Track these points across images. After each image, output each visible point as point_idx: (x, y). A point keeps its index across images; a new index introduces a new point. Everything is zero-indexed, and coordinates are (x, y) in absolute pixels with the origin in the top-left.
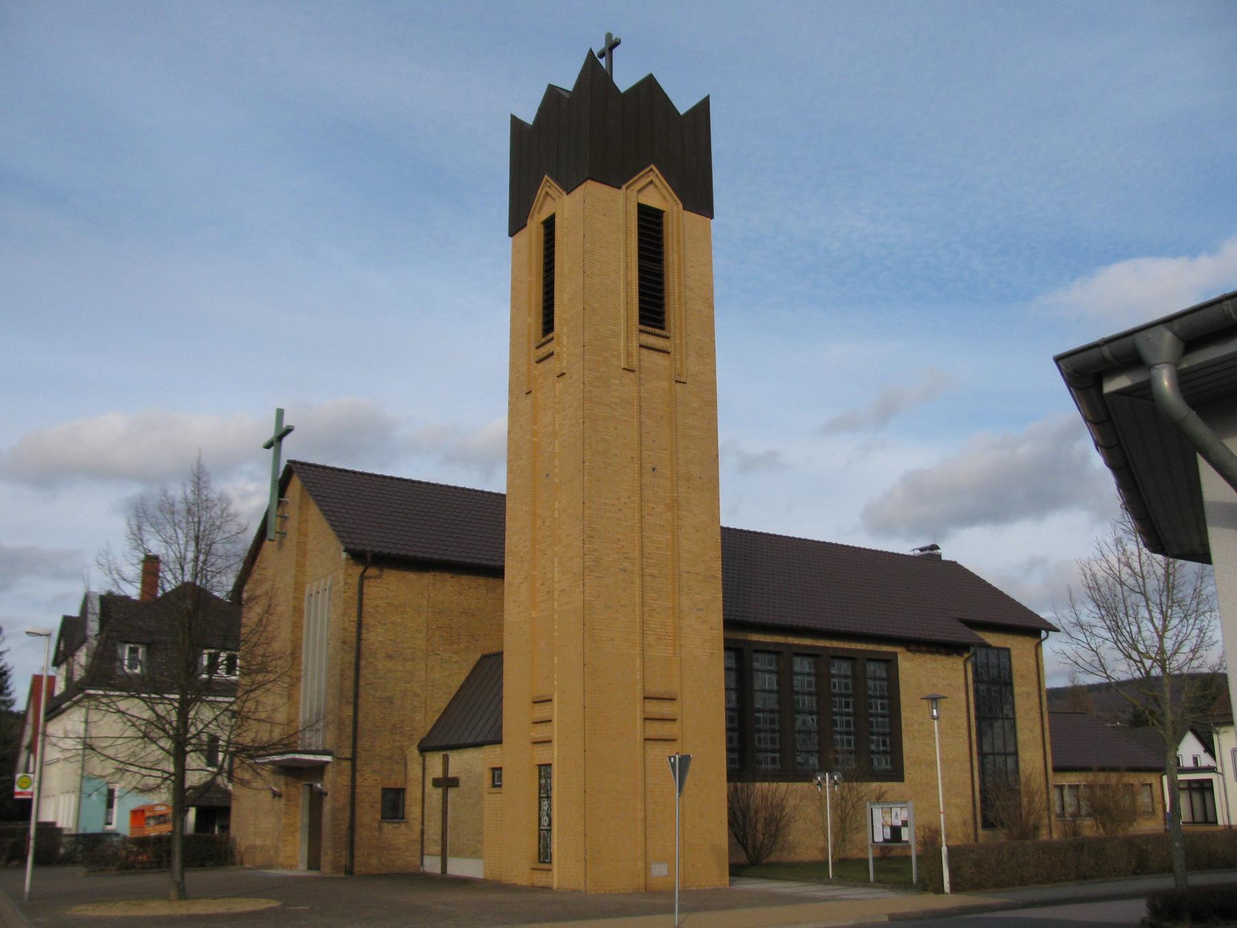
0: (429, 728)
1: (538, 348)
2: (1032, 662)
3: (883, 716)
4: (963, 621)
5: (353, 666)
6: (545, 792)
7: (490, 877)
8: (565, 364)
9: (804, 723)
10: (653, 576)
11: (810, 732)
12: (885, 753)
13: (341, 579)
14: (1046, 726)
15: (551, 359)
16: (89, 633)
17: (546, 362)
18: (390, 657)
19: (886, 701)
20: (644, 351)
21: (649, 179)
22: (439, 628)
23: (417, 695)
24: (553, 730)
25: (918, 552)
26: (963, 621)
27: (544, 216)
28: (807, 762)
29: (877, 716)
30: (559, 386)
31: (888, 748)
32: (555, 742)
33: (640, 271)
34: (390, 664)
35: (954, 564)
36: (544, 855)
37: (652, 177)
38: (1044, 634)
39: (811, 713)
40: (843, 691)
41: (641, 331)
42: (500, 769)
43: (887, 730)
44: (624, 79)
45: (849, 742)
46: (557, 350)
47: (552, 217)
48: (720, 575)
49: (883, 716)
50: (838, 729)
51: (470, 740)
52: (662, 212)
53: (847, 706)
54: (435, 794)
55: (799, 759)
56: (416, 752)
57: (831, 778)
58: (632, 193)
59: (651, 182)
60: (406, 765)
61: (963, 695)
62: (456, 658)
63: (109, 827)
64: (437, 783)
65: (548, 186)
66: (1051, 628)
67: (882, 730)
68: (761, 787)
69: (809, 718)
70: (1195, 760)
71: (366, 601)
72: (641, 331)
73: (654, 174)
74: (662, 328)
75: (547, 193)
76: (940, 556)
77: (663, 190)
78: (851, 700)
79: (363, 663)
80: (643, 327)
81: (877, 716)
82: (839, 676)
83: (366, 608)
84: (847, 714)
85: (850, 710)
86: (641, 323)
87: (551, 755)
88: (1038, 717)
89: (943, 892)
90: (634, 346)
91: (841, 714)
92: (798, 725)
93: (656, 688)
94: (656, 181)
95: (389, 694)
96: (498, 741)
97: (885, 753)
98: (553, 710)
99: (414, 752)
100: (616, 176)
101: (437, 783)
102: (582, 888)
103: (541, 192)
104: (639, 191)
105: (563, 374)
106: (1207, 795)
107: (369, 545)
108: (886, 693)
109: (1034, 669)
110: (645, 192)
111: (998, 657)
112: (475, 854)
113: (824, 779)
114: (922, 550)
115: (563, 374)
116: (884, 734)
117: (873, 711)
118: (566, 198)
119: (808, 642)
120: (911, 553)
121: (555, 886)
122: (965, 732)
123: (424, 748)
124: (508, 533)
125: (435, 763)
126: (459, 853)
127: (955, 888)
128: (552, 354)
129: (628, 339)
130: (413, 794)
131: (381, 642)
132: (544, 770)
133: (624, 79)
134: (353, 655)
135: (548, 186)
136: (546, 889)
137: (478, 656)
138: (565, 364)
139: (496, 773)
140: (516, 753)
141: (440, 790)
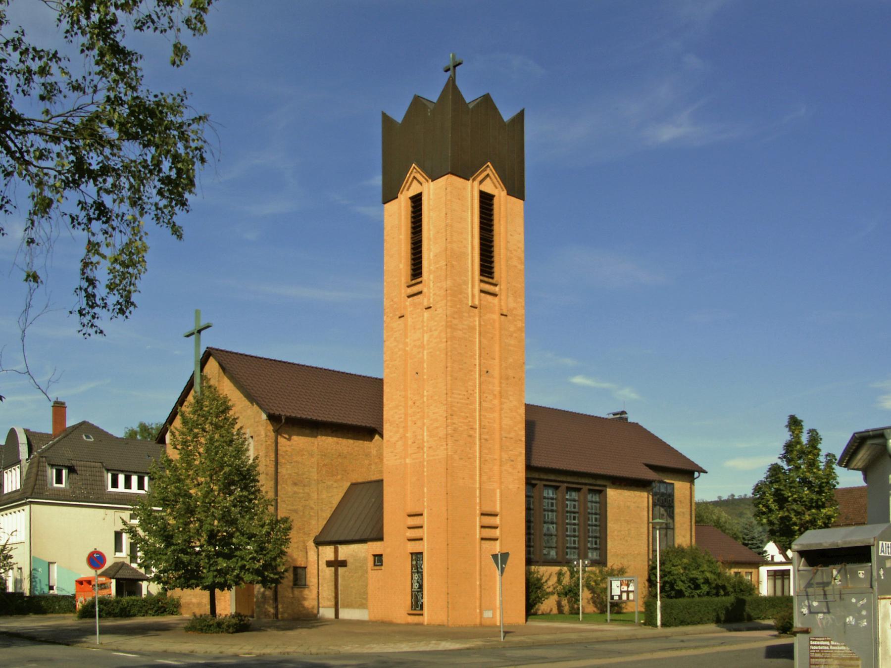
0: (320, 529)
1: (408, 287)
2: (688, 493)
3: (596, 526)
4: (647, 465)
5: (273, 490)
6: (417, 569)
7: (373, 619)
8: (431, 300)
9: (548, 529)
10: (486, 440)
11: (551, 535)
12: (596, 549)
13: (263, 433)
14: (693, 534)
15: (419, 296)
16: (21, 458)
17: (415, 297)
18: (295, 484)
19: (598, 516)
20: (483, 295)
21: (485, 173)
22: (324, 465)
23: (312, 508)
24: (424, 533)
25: (611, 416)
26: (647, 465)
27: (412, 192)
28: (549, 554)
29: (592, 525)
30: (426, 314)
31: (598, 546)
32: (425, 539)
33: (481, 239)
34: (296, 489)
35: (636, 425)
36: (417, 605)
37: (488, 171)
38: (696, 474)
39: (552, 523)
40: (573, 510)
41: (481, 281)
42: (381, 555)
43: (598, 535)
44: (470, 96)
45: (574, 541)
46: (425, 290)
47: (420, 194)
48: (523, 439)
49: (596, 526)
50: (568, 533)
51: (357, 538)
52: (493, 196)
53: (574, 519)
54: (329, 572)
55: (545, 552)
56: (313, 544)
57: (583, 563)
58: (476, 183)
59: (488, 175)
60: (307, 553)
61: (646, 514)
62: (335, 485)
63: (51, 592)
64: (329, 564)
65: (414, 171)
66: (702, 471)
67: (595, 534)
68: (533, 567)
69: (551, 526)
70: (773, 557)
71: (279, 448)
72: (481, 281)
73: (490, 169)
74: (492, 278)
75: (414, 178)
76: (626, 419)
77: (495, 180)
78: (577, 515)
79: (279, 487)
80: (482, 278)
81: (592, 525)
82: (570, 500)
83: (280, 452)
84: (575, 524)
85: (576, 522)
86: (481, 275)
87: (423, 547)
88: (689, 528)
89: (656, 626)
90: (477, 291)
91: (570, 524)
92: (545, 529)
93: (487, 509)
94: (491, 175)
95: (295, 507)
96: (380, 538)
97: (596, 549)
98: (425, 520)
99: (311, 544)
100: (466, 172)
101: (329, 564)
102: (446, 623)
103: (409, 176)
104: (481, 182)
105: (430, 307)
106: (786, 581)
107: (286, 412)
108: (598, 511)
109: (689, 498)
110: (484, 183)
111: (666, 488)
112: (363, 606)
113: (578, 564)
114: (614, 414)
115: (430, 307)
116: (596, 537)
117: (590, 523)
118: (432, 185)
119: (552, 477)
120: (606, 416)
121: (426, 623)
122: (645, 537)
123: (319, 543)
124: (385, 408)
125: (328, 553)
126: (348, 606)
127: (664, 625)
128: (420, 293)
129: (473, 286)
130: (312, 571)
131: (290, 474)
132: (417, 557)
133: (470, 96)
134: (273, 482)
135: (414, 171)
136: (422, 624)
137: (349, 484)
138: (431, 300)
139: (378, 559)
140: (395, 545)
141: (333, 569)
